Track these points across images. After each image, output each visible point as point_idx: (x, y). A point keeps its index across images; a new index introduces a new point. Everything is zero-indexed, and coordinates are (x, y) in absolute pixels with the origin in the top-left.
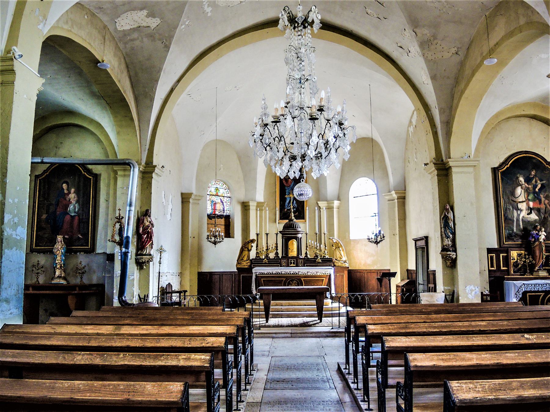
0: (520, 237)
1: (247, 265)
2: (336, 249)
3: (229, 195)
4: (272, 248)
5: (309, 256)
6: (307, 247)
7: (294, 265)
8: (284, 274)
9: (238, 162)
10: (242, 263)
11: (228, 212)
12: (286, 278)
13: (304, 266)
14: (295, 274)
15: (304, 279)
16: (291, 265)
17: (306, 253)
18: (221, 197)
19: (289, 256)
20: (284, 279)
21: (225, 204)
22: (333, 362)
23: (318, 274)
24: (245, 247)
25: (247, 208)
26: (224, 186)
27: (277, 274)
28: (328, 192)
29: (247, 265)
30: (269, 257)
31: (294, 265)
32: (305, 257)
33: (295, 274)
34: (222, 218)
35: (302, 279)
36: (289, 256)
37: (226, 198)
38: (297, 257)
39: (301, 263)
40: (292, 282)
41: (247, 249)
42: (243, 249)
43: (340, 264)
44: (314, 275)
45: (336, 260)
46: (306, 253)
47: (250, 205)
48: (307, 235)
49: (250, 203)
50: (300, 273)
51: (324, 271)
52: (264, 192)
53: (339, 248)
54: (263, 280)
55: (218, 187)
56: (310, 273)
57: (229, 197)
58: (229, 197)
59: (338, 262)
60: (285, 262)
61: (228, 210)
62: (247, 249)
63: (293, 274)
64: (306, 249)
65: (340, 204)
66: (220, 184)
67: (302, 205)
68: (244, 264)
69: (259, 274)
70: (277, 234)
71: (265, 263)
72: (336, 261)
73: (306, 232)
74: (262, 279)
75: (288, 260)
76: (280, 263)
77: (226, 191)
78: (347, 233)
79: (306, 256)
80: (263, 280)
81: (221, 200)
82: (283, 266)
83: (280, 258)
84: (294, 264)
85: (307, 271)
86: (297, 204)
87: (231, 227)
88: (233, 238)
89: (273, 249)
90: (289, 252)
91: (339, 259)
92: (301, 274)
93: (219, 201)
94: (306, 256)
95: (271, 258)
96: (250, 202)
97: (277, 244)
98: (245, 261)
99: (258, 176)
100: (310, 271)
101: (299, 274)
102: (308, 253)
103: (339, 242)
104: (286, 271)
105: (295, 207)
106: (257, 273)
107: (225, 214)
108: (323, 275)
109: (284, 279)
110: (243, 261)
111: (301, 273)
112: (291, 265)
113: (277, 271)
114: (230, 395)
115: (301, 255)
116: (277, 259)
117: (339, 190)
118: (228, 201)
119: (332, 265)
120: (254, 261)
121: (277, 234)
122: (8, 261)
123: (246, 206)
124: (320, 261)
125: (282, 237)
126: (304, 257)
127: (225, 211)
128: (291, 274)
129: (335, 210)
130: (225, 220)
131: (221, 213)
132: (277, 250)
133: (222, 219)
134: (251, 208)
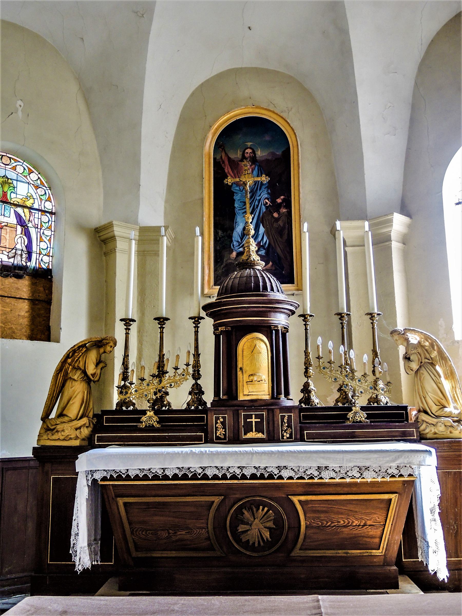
0: (434, 367)
1: (77, 438)
2: (423, 371)
3: (49, 206)
4: (176, 368)
5: (316, 400)
6: (307, 365)
7: (260, 435)
8: (215, 477)
9: (82, 106)
10: (58, 427)
11: (46, 259)
12: (226, 496)
13: (302, 439)
14: (262, 477)
15: (303, 498)
16: (250, 435)
17: (306, 389)
18: (19, 210)
19: (241, 398)
20: (217, 500)
21: (33, 231)
22: (282, 471)
23: (369, 477)
24: (74, 368)
25: (110, 245)
26: (34, 176)
27: (185, 477)
28: (367, 193)
29: (77, 438)
30: (169, 404)
31: (260, 435)
32: (301, 402)
33: (262, 477)
34: (19, 277)
35: (295, 499)
36: (241, 398)
37: (37, 215)
38: (272, 404)
39: (289, 426)
40: (250, 509)
41: (79, 372)
42: (66, 373)
43: (441, 429)
44: (348, 480)
45: (426, 412)
46: (306, 389)
47: (116, 233)
48: (305, 320)
49: (115, 228)
50: (285, 474)
51: (394, 465)
52: (167, 201)
53: (433, 365)
54: (125, 504)
55: (11, 175)
56: (333, 474)
57: (51, 213)
58: (51, 213)
59: (434, 421)
60: (223, 423)
61: (44, 252)
62: (79, 372)
63: (253, 477)
64: (306, 372)
65: (410, 226)
66: (20, 169)
67: (285, 237)
68: (67, 433)
69: (104, 479)
70: (197, 320)
71: (150, 429)
72: (423, 417)
73: (304, 310)
74: (121, 501)
75: (236, 415)
76: (204, 429)
77: (41, 191)
78: (441, 322)
79: (307, 400)
80: (125, 504)
81: (18, 216)
82: (218, 438)
83: (209, 405)
84: (259, 430)
85: (315, 465)
86: (268, 238)
87: (53, 307)
88: (58, 341)
89: (179, 371)
90: (240, 384)
91: (434, 408)
92: (291, 478)
93: (13, 220)
94: (307, 400)
95: (174, 407)
96: (114, 223)
97: (197, 355)
98: (72, 421)
99: (145, 148)
100: (332, 465)
101: (281, 478)
102: (312, 387)
103: (432, 345)
104: (226, 465)
105: (263, 247)
106: (98, 476)
107: (32, 264)
108: (388, 479)
109: (217, 500)
110: (66, 419)
111: (292, 474)
112: (250, 435)
113: (186, 466)
114: (224, 433)
115: (287, 394)
116: (196, 411)
117: (404, 185)
118: (45, 226)
119: (411, 434)
120: (108, 420)
121: (197, 320)
122: (256, 382)
123: (104, 241)
124: (362, 416)
125: (216, 327)
126: (297, 404)
127: (34, 256)
128: (244, 477)
129: (395, 246)
130: (33, 285)
131: (17, 261)
132: (197, 376)
133: (21, 281)
134: (120, 245)
